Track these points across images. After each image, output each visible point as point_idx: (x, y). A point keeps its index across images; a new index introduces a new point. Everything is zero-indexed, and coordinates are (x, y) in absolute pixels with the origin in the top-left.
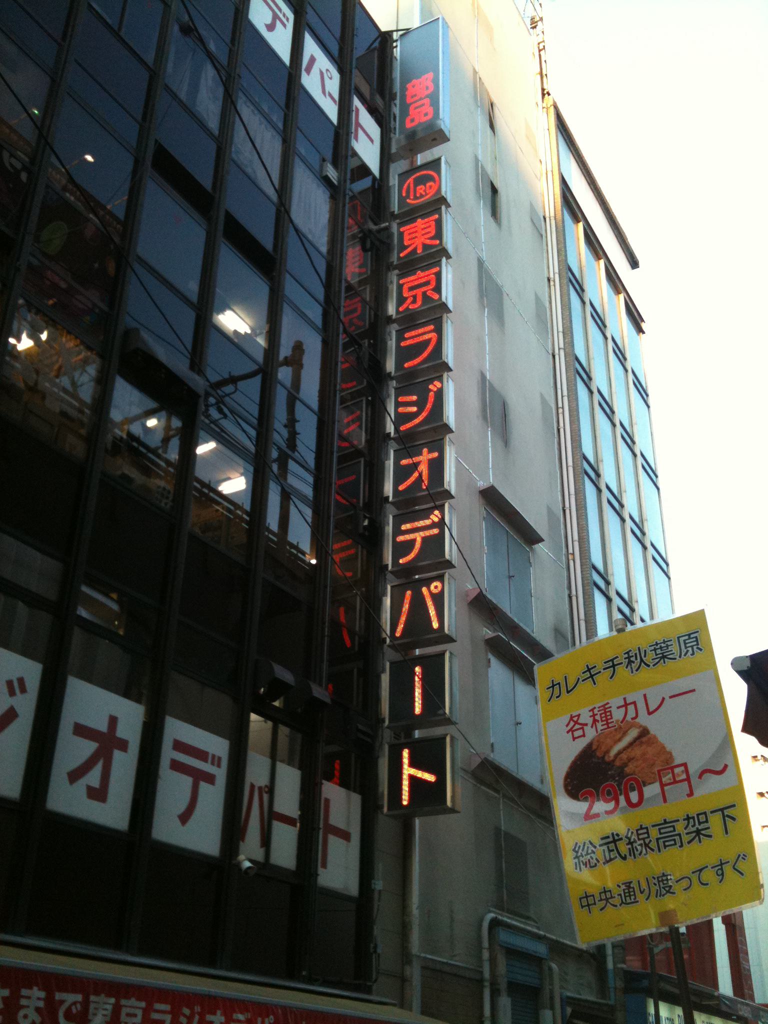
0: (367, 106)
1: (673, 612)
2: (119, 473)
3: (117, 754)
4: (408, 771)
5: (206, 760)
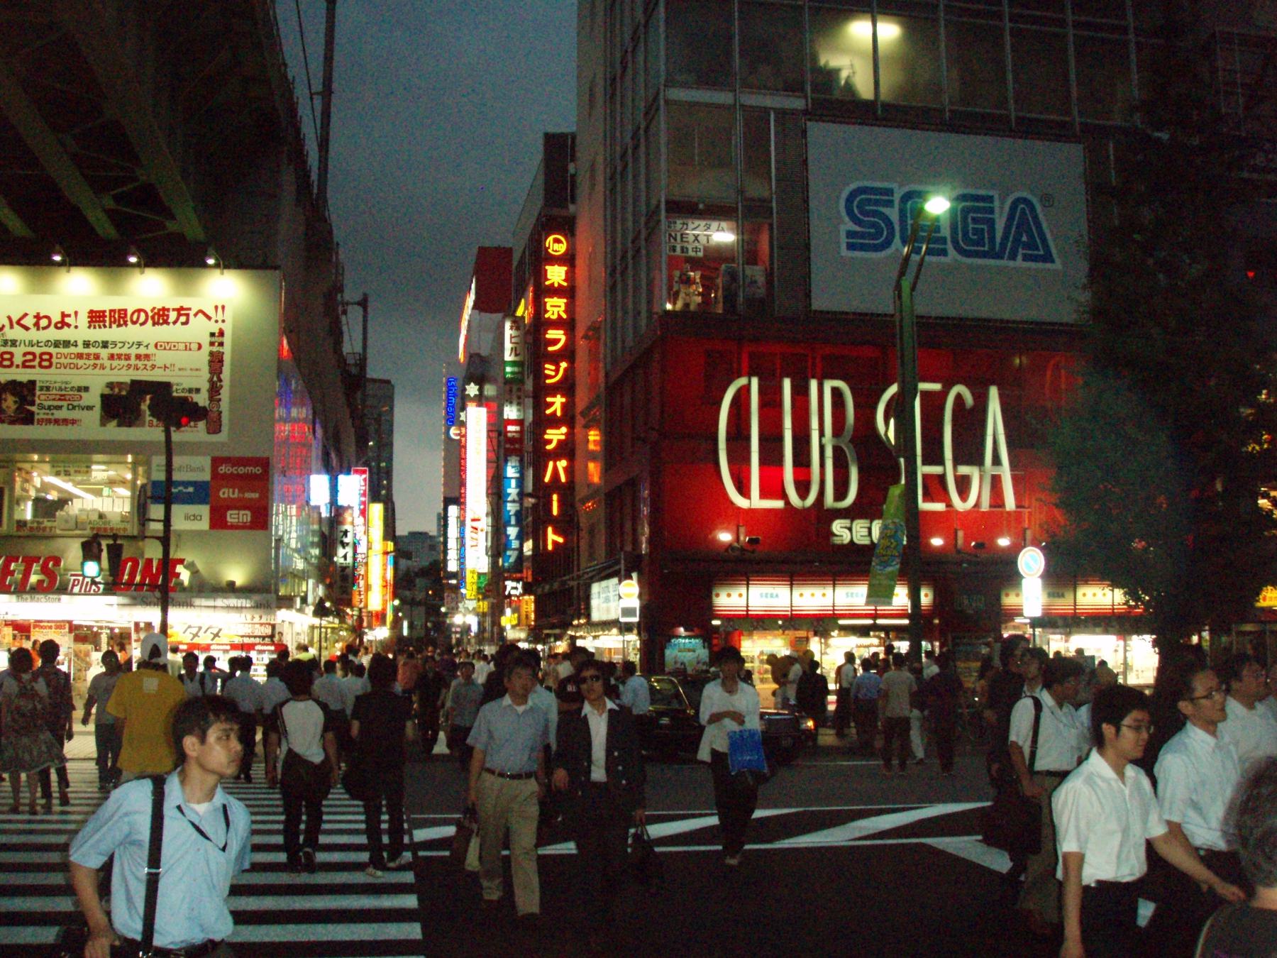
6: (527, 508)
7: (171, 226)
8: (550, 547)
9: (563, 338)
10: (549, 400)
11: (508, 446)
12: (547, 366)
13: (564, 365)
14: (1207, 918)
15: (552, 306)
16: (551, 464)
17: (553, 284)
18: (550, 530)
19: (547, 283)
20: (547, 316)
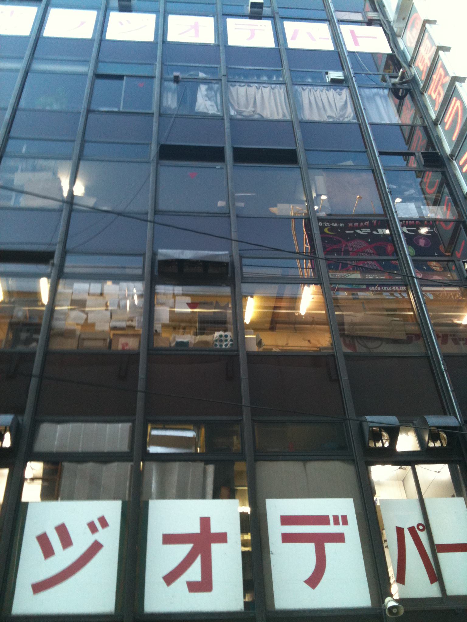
0: (248, 18)
1: (328, 39)
2: (173, 344)
3: (216, 548)
5: (328, 523)
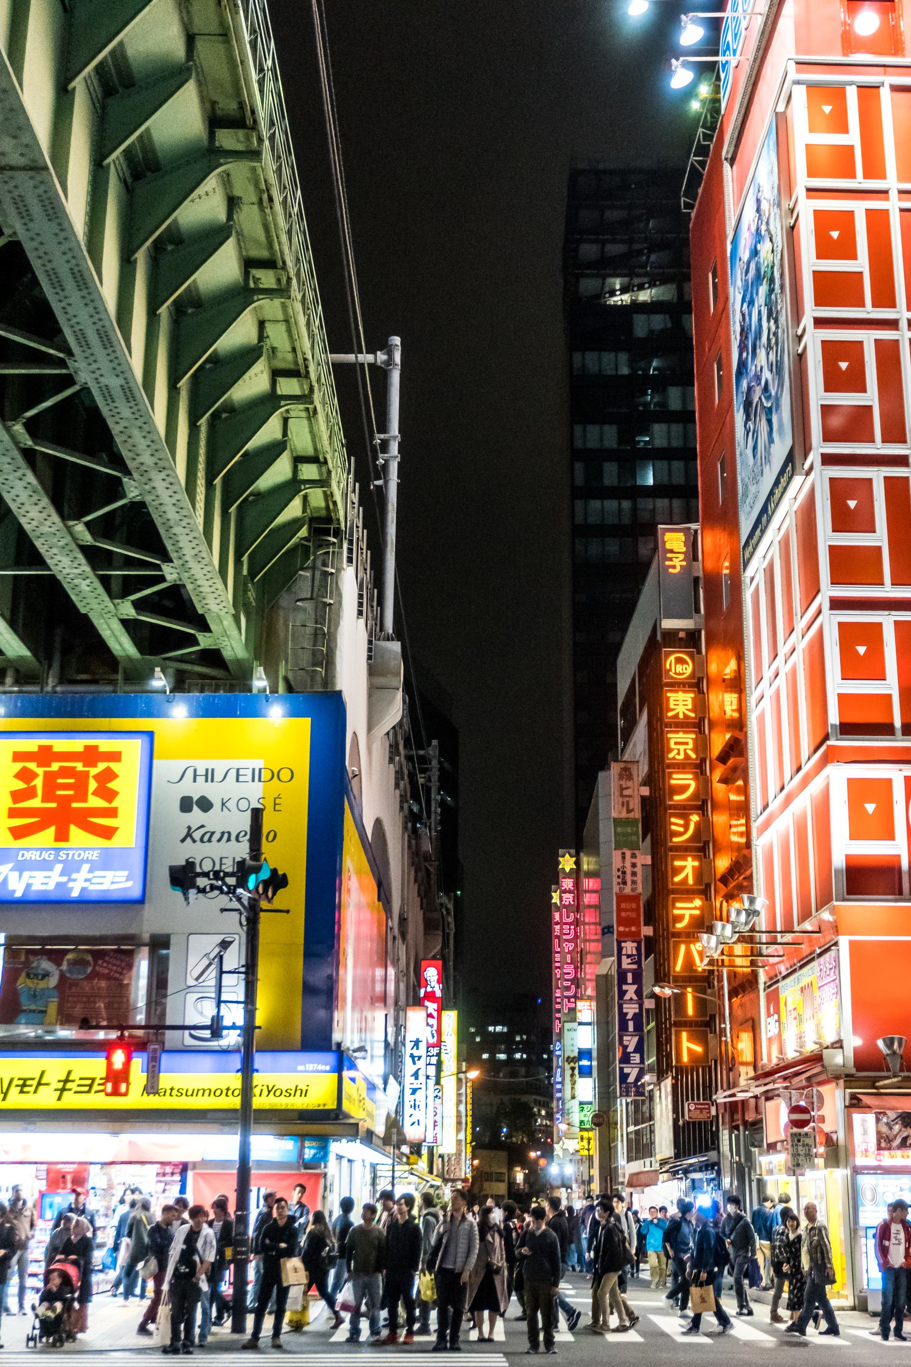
4: (324, 649)
6: (648, 1010)
7: (204, 641)
8: (685, 1058)
9: (693, 785)
10: (677, 863)
11: (621, 929)
12: (673, 820)
13: (695, 818)
14: (384, 1296)
15: (676, 743)
16: (683, 947)
17: (677, 715)
18: (684, 1035)
19: (670, 714)
20: (671, 756)
